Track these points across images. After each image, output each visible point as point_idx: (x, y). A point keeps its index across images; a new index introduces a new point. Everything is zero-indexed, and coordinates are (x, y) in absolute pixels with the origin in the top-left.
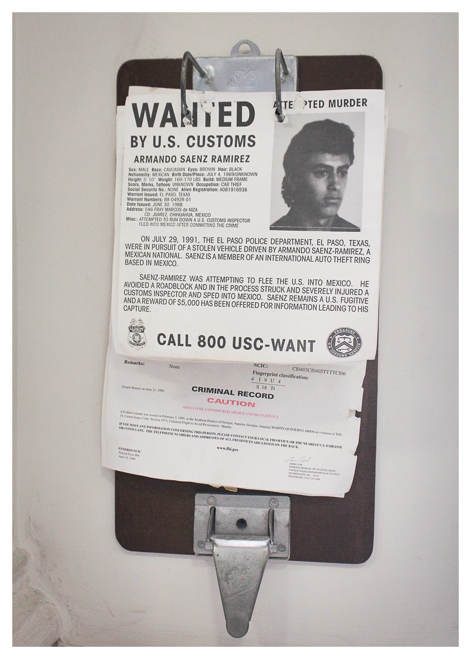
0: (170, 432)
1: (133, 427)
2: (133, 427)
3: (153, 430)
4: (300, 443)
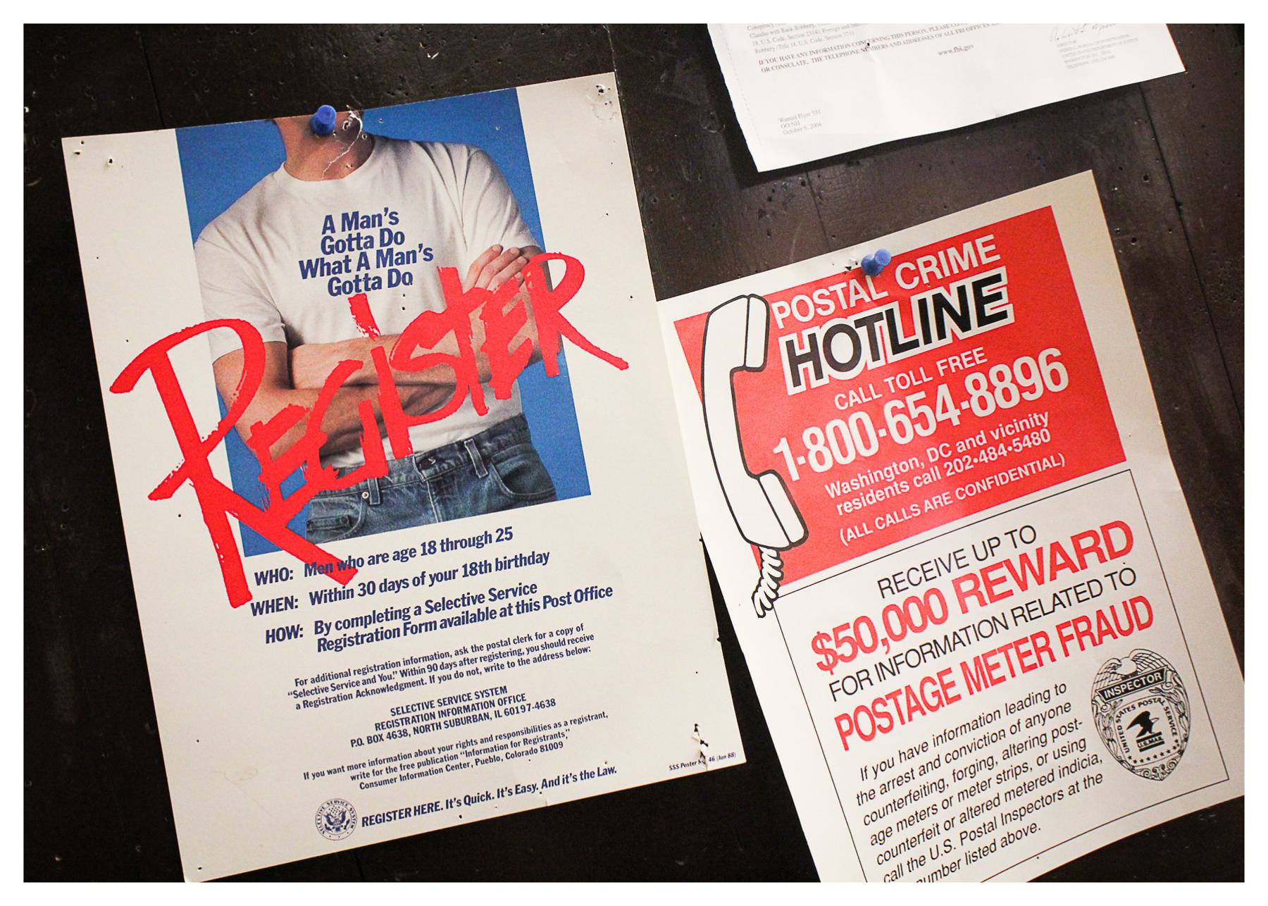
0: (851, 48)
1: (786, 62)
2: (786, 62)
3: (822, 55)
4: (370, 740)
